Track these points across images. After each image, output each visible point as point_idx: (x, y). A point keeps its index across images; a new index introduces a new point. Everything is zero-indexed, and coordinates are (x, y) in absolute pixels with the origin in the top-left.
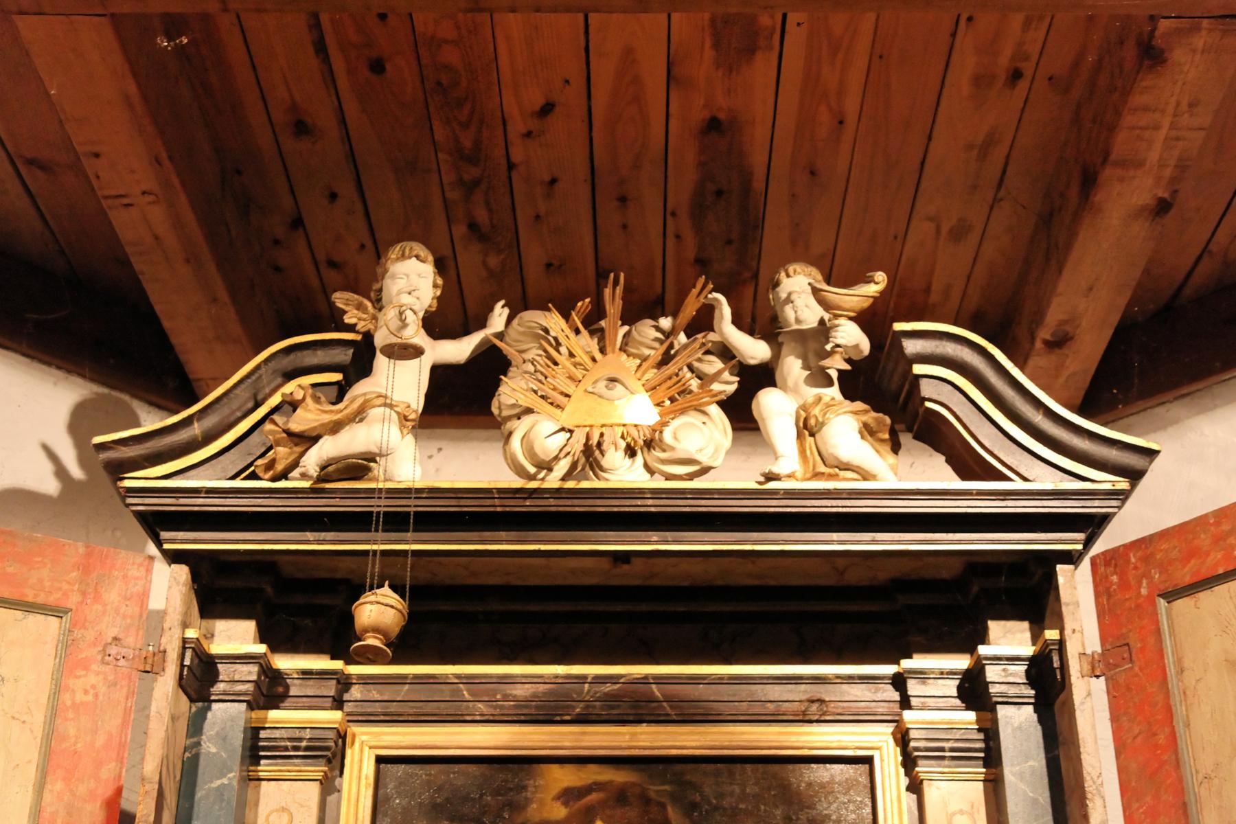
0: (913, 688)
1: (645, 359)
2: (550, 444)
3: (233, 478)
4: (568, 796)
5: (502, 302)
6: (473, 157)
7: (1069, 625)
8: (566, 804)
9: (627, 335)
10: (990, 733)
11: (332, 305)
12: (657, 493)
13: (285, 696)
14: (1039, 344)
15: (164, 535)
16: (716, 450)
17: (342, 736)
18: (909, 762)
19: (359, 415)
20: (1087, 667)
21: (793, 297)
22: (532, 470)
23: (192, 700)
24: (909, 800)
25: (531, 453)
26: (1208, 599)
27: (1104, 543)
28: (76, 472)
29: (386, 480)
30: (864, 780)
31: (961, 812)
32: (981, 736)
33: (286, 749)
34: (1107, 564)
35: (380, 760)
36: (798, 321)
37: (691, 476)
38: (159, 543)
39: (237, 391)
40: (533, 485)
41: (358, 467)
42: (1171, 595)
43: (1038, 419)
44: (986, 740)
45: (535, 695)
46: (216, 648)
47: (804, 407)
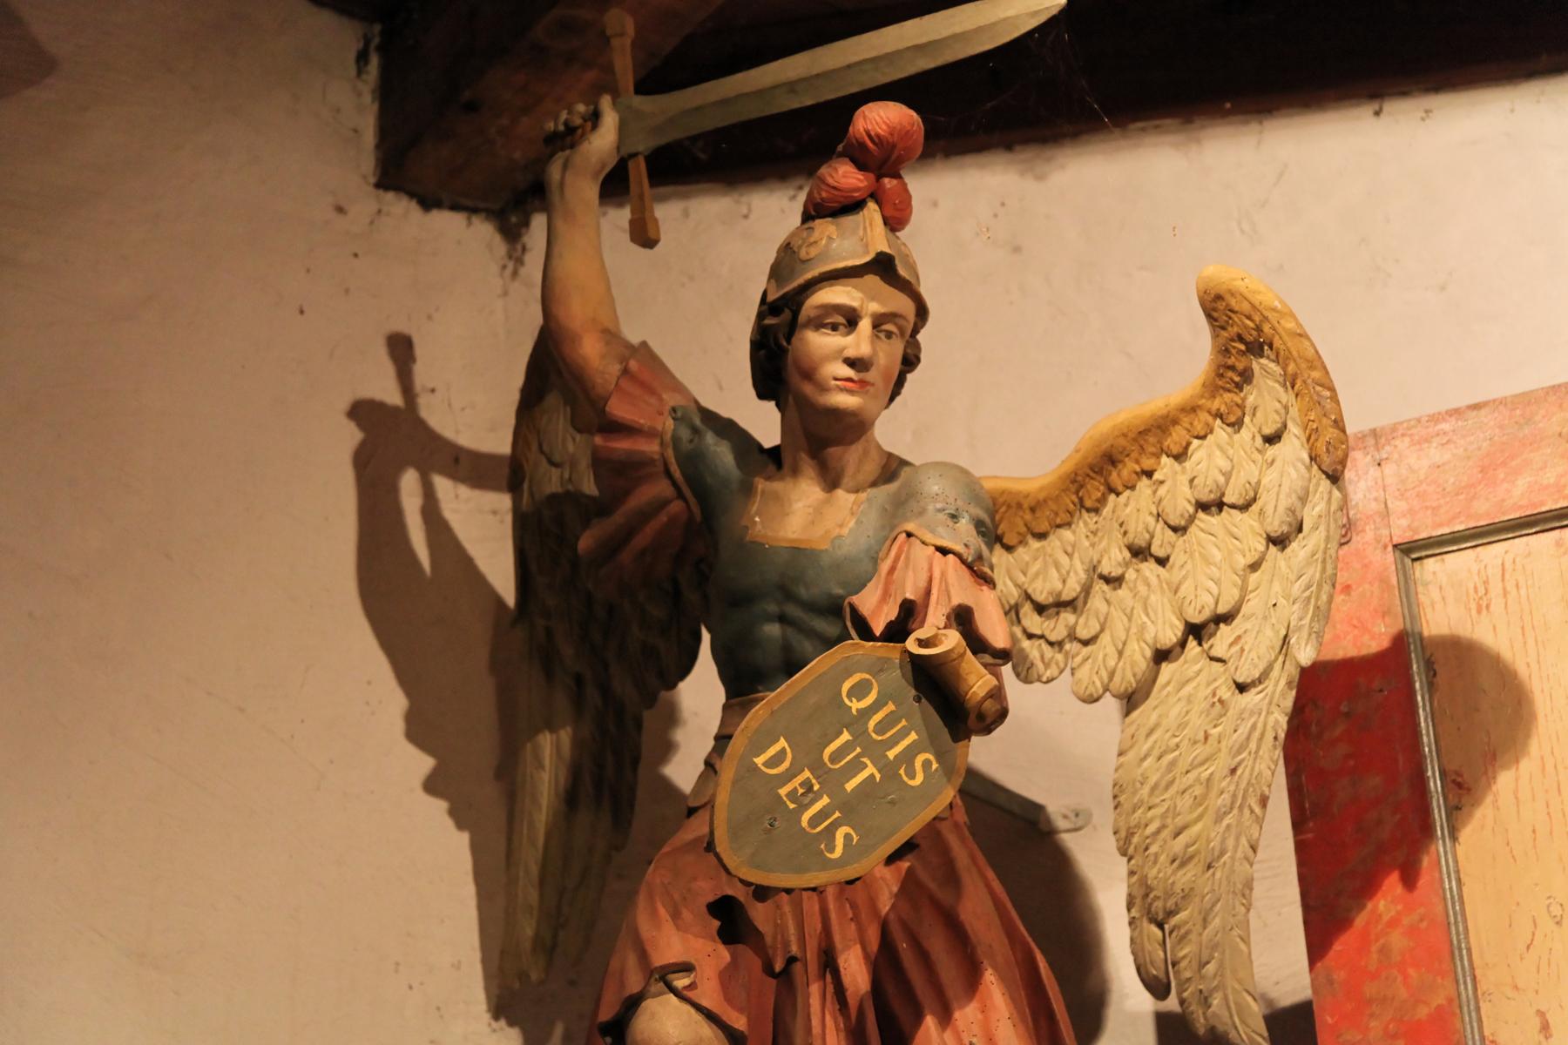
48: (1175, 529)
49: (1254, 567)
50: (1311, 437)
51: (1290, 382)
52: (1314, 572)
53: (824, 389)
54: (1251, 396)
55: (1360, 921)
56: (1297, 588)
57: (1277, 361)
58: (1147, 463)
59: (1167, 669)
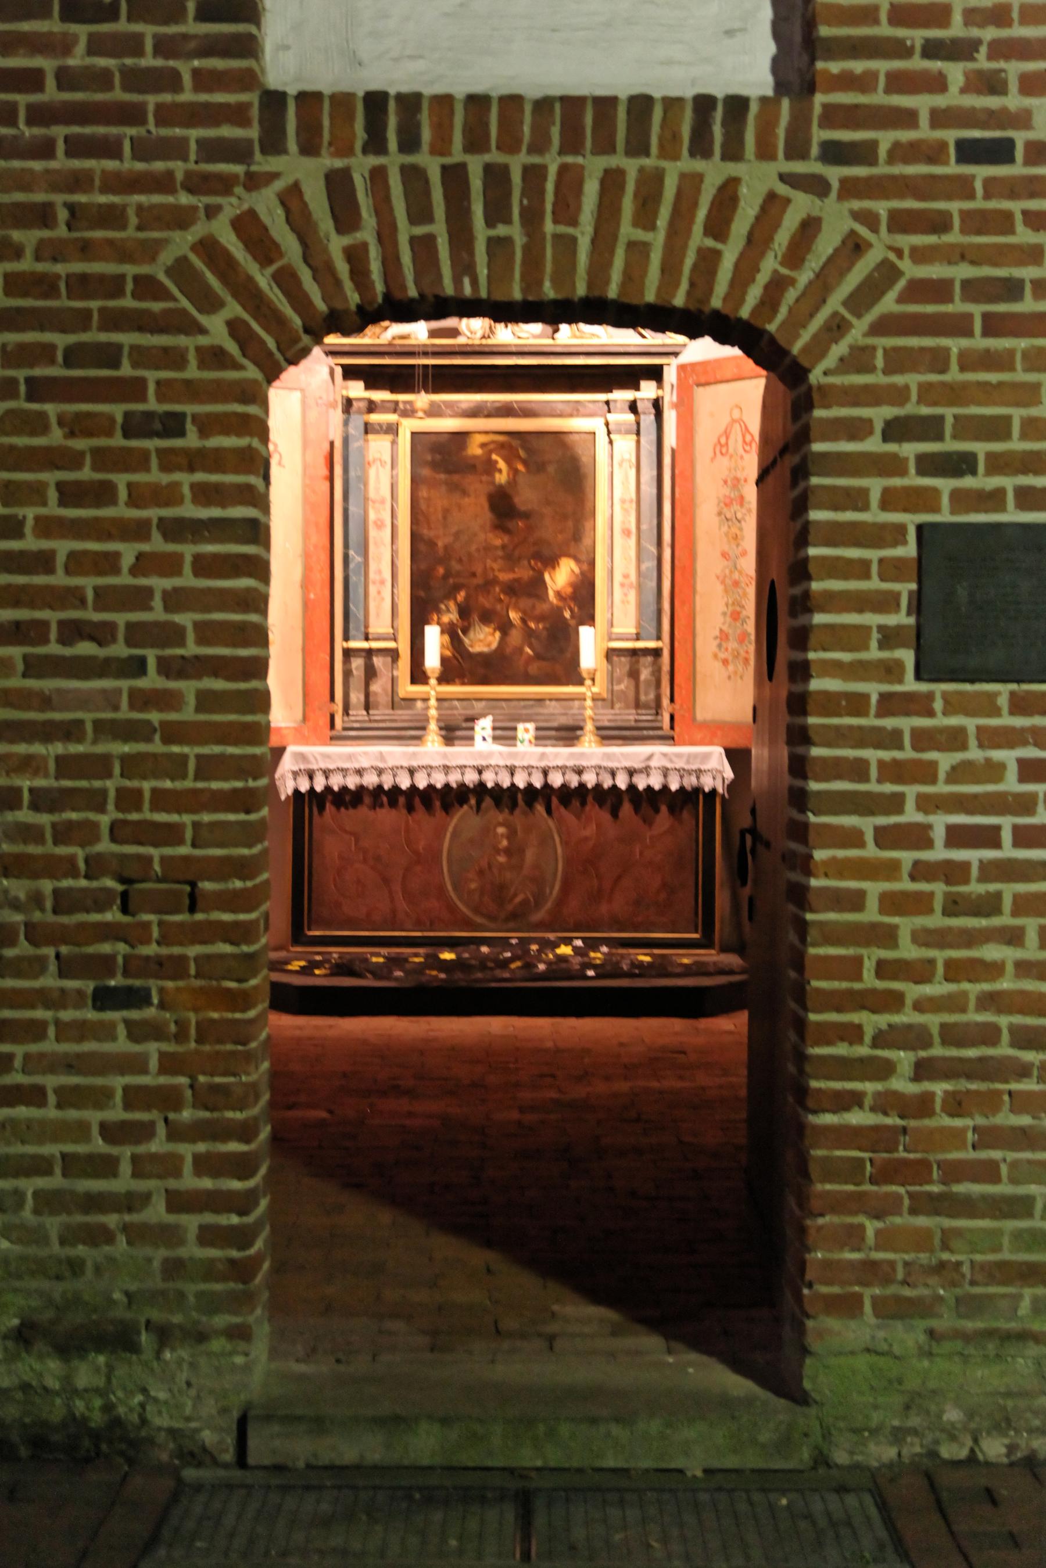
4: (483, 445)
18: (609, 433)
35: (413, 433)
42: (699, 385)
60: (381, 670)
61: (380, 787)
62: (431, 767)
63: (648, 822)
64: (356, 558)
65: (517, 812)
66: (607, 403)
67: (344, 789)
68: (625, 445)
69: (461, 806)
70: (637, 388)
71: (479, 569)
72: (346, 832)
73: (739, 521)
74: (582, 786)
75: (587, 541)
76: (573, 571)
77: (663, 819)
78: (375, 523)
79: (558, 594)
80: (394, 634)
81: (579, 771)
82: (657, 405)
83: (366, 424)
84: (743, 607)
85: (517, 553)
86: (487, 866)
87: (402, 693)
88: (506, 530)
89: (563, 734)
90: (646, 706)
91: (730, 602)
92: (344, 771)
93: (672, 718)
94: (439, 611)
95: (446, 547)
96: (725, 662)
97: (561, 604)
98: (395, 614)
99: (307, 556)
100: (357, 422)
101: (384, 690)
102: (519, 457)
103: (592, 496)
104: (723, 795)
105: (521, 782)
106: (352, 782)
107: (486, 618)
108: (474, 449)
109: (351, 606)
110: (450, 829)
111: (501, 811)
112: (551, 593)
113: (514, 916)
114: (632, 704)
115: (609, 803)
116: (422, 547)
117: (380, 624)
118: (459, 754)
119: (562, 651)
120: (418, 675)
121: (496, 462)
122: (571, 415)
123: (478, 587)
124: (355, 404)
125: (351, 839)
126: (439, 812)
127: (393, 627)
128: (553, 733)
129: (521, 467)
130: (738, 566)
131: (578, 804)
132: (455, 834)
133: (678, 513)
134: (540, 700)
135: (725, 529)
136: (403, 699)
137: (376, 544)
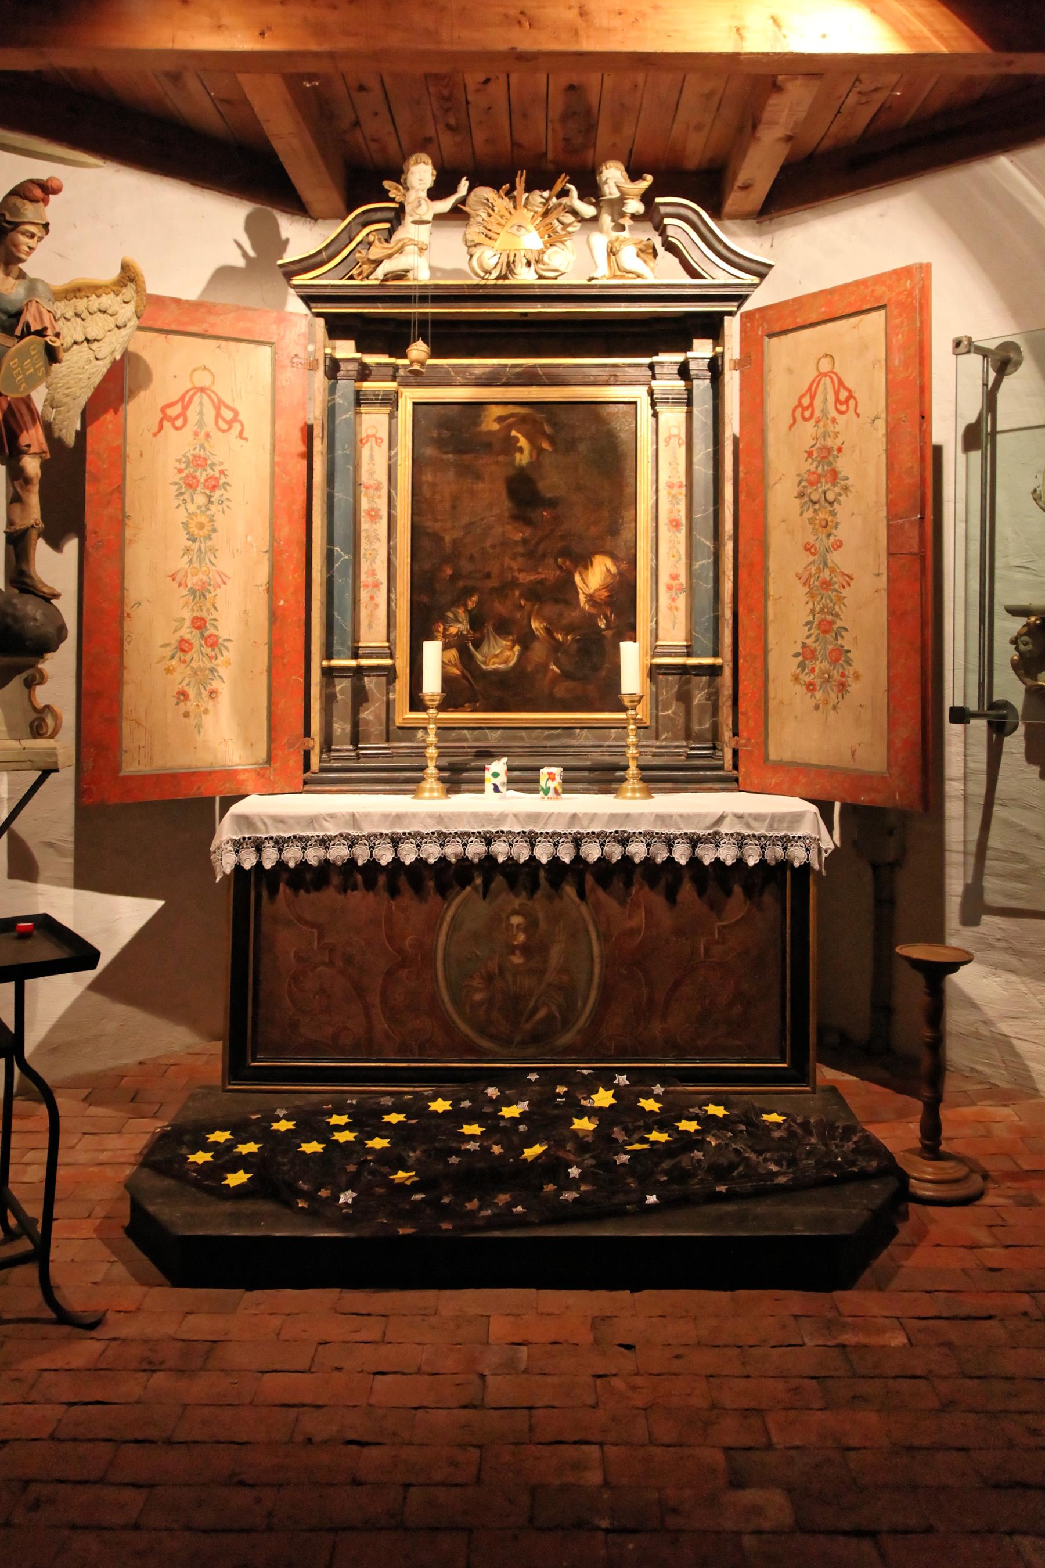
0: (657, 370)
1: (536, 212)
2: (490, 261)
3: (341, 279)
4: (500, 419)
5: (465, 178)
6: (448, 99)
7: (727, 345)
8: (499, 423)
9: (527, 198)
10: (689, 391)
11: (383, 187)
12: (540, 286)
13: (369, 375)
14: (735, 187)
15: (312, 305)
16: (568, 264)
17: (397, 393)
18: (653, 404)
19: (400, 251)
20: (732, 365)
21: (608, 181)
22: (482, 274)
23: (329, 379)
24: (652, 420)
25: (481, 266)
26: (784, 339)
27: (748, 306)
28: (252, 253)
29: (414, 280)
30: (633, 412)
31: (675, 427)
32: (686, 392)
33: (372, 400)
34: (746, 317)
35: (414, 404)
36: (610, 194)
37: (556, 278)
38: (310, 308)
39: (342, 235)
40: (483, 282)
41: (401, 275)
42: (771, 336)
43: (720, 248)
44: (688, 394)
45: (483, 373)
46: (338, 355)
47: (611, 242)
48: (90, 313)
49: (110, 331)
50: (137, 307)
51: (137, 292)
52: (126, 338)
53: (19, 251)
54: (124, 290)
55: (102, 419)
56: (121, 340)
57: (136, 285)
58: (88, 295)
59: (75, 347)
60: (373, 692)
61: (352, 861)
62: (422, 836)
63: (716, 908)
64: (342, 556)
65: (538, 894)
66: (651, 366)
67: (303, 865)
68: (673, 418)
69: (463, 888)
70: (689, 347)
71: (494, 567)
72: (306, 923)
73: (831, 503)
74: (627, 859)
75: (626, 535)
76: (608, 570)
77: (737, 904)
78: (368, 513)
79: (590, 598)
80: (389, 648)
81: (623, 840)
82: (715, 367)
83: (358, 392)
84: (837, 615)
85: (541, 548)
86: (497, 971)
87: (399, 722)
88: (528, 522)
89: (596, 775)
90: (700, 738)
91: (818, 609)
92: (304, 842)
93: (735, 753)
94: (445, 621)
95: (455, 542)
96: (810, 687)
97: (594, 611)
98: (392, 624)
99: (275, 553)
100: (346, 387)
101: (377, 717)
102: (544, 433)
103: (633, 481)
104: (820, 871)
105: (543, 854)
106: (314, 856)
107: (503, 628)
108: (490, 423)
109: (336, 614)
110: (448, 918)
111: (517, 896)
112: (582, 598)
113: (536, 1038)
114: (682, 733)
115: (663, 882)
116: (426, 543)
117: (373, 636)
118: (463, 803)
119: (595, 669)
120: (417, 703)
121: (517, 440)
122: (607, 384)
123: (493, 590)
124: (343, 366)
125: (313, 933)
126: (434, 898)
127: (388, 640)
128: (586, 774)
129: (546, 445)
130: (830, 563)
131: (621, 885)
132: (455, 925)
133: (742, 497)
134: (569, 728)
135: (809, 514)
136: (400, 728)
137: (367, 537)
